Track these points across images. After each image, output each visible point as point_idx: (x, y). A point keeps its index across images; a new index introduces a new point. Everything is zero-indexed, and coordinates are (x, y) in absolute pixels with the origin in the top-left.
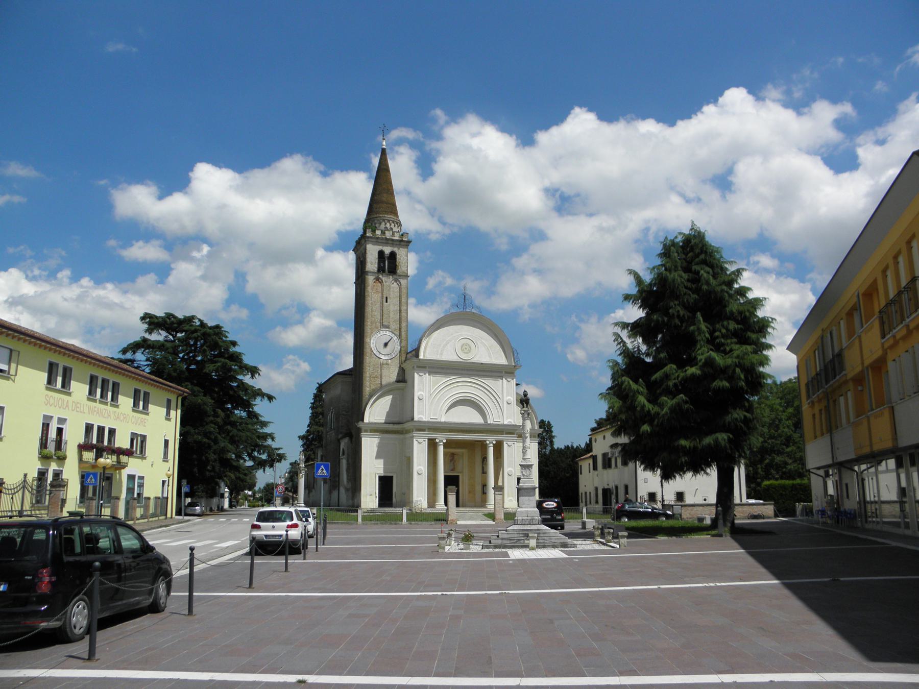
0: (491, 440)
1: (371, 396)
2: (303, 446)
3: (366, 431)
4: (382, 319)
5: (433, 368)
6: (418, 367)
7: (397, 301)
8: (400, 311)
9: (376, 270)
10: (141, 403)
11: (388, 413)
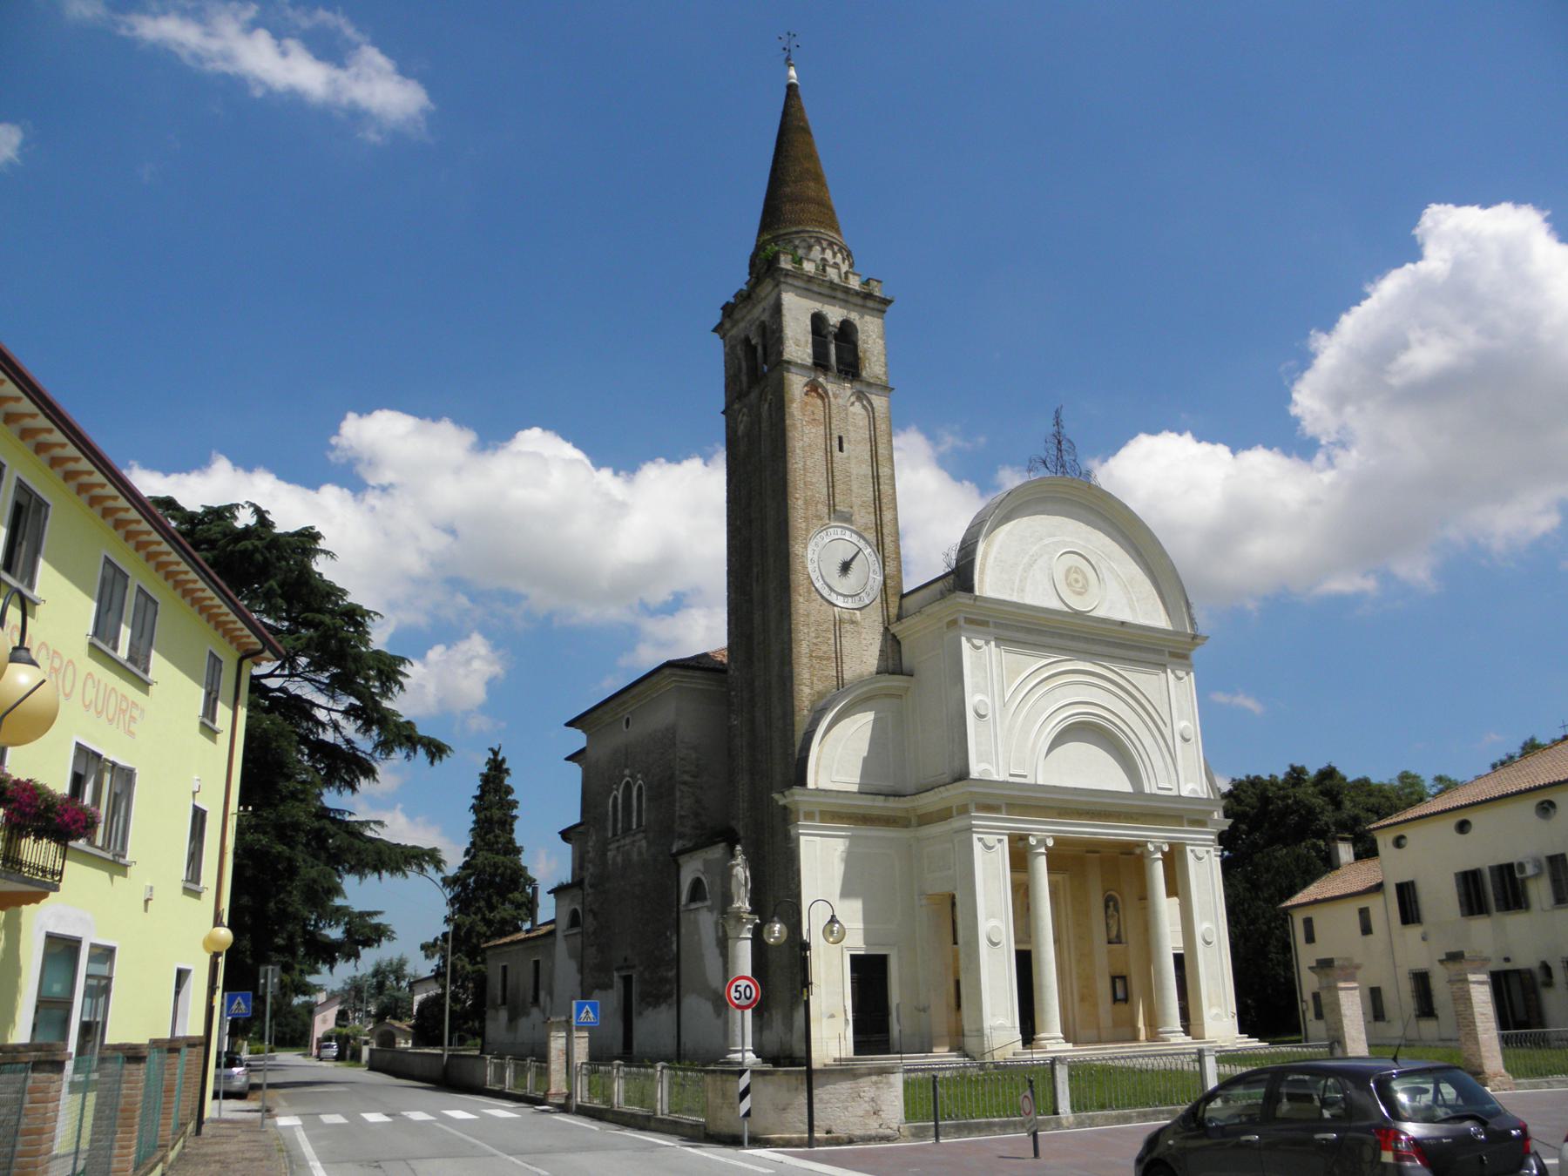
0: (1155, 838)
2: (452, 902)
3: (809, 816)
4: (831, 495)
5: (1006, 627)
6: (969, 621)
7: (864, 451)
8: (876, 478)
9: (809, 361)
10: (125, 633)
11: (865, 760)
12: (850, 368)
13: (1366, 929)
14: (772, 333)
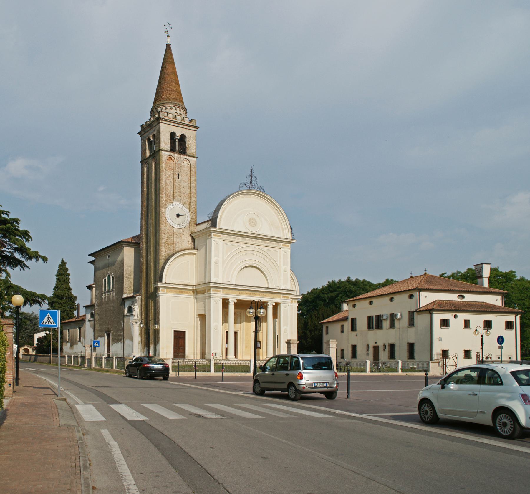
0: (271, 301)
1: (167, 260)
7: (192, 175)
9: (169, 149)
12: (183, 151)
13: (342, 332)
14: (157, 137)
